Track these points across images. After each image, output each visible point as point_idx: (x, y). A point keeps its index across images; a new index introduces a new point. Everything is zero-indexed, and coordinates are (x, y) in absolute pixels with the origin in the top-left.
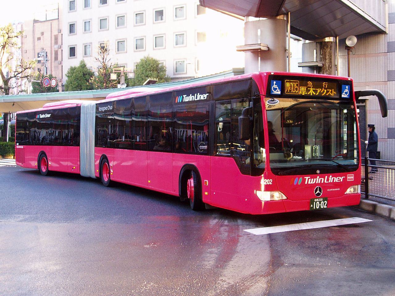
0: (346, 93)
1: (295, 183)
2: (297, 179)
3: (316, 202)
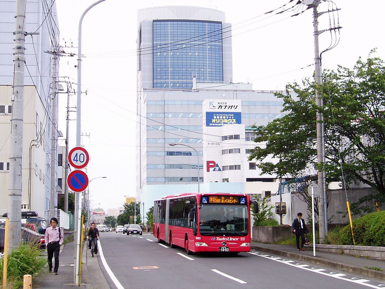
0: (243, 201)
1: (212, 240)
2: (213, 238)
3: (222, 248)
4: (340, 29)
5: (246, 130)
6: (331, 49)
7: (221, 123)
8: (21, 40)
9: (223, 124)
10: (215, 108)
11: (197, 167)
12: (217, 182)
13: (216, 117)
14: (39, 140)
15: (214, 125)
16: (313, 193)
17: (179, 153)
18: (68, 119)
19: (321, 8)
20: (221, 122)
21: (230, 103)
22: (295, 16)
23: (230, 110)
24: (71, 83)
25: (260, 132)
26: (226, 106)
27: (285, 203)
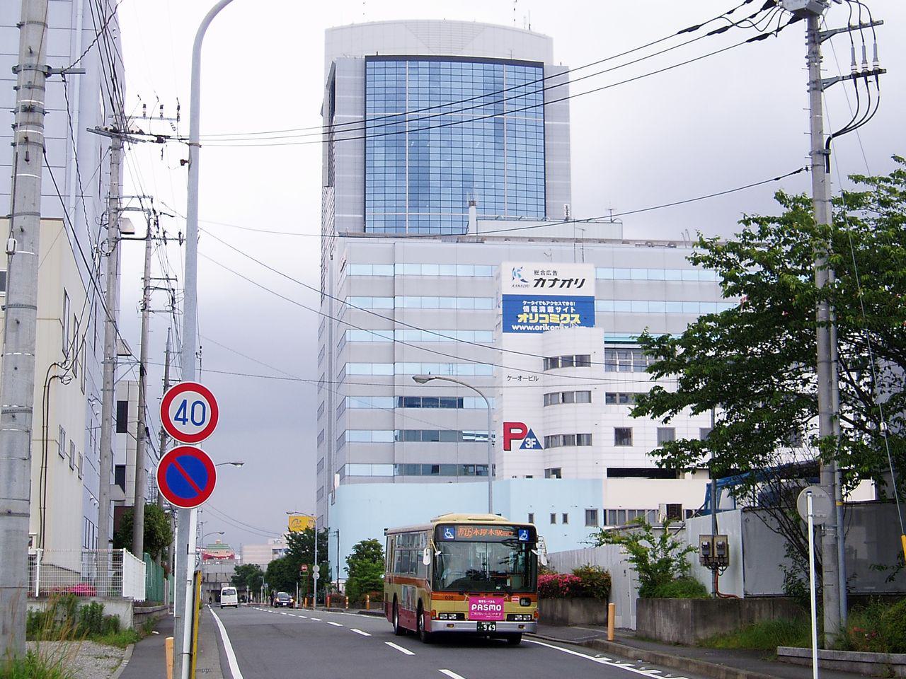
4: (879, 75)
5: (606, 342)
6: (855, 127)
7: (542, 324)
8: (34, 87)
9: (547, 328)
10: (526, 286)
11: (486, 439)
12: (531, 477)
13: (528, 307)
14: (69, 364)
15: (523, 328)
16: (810, 513)
17: (431, 402)
18: (147, 309)
19: (832, 17)
20: (541, 321)
21: (565, 272)
22: (757, 41)
23: (565, 292)
24: (158, 214)
25: (663, 351)
26: (556, 279)
27: (727, 536)
